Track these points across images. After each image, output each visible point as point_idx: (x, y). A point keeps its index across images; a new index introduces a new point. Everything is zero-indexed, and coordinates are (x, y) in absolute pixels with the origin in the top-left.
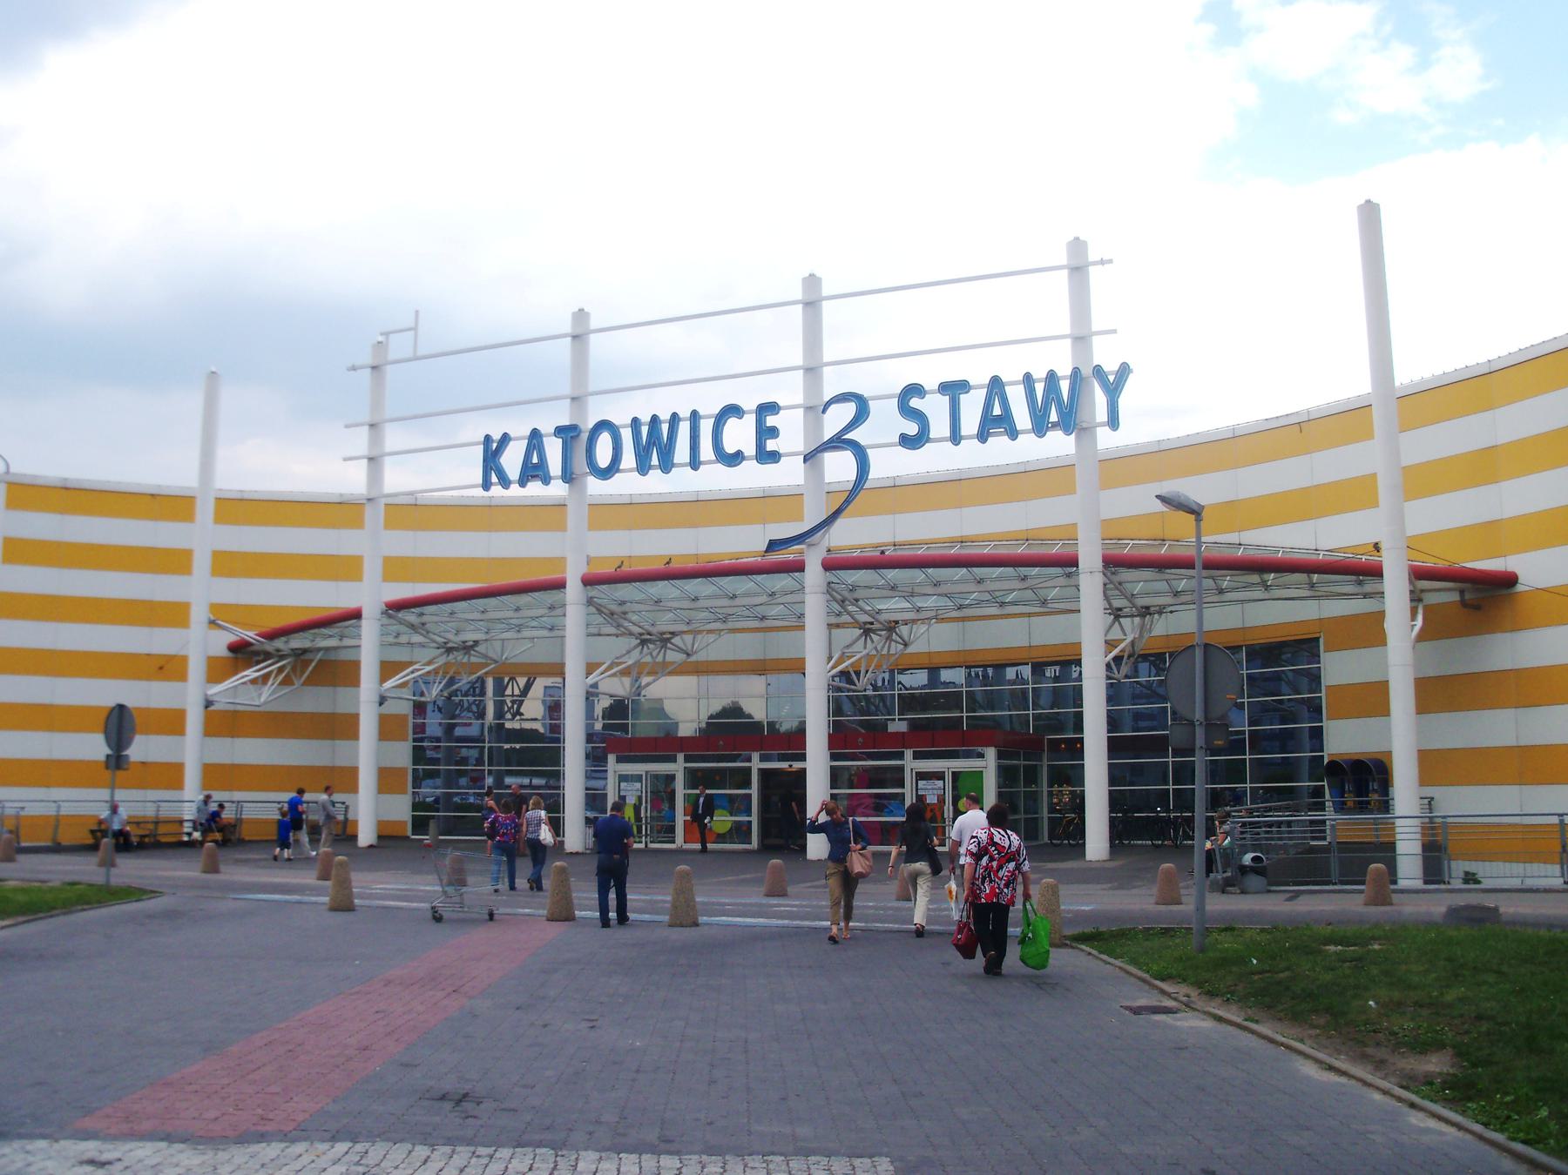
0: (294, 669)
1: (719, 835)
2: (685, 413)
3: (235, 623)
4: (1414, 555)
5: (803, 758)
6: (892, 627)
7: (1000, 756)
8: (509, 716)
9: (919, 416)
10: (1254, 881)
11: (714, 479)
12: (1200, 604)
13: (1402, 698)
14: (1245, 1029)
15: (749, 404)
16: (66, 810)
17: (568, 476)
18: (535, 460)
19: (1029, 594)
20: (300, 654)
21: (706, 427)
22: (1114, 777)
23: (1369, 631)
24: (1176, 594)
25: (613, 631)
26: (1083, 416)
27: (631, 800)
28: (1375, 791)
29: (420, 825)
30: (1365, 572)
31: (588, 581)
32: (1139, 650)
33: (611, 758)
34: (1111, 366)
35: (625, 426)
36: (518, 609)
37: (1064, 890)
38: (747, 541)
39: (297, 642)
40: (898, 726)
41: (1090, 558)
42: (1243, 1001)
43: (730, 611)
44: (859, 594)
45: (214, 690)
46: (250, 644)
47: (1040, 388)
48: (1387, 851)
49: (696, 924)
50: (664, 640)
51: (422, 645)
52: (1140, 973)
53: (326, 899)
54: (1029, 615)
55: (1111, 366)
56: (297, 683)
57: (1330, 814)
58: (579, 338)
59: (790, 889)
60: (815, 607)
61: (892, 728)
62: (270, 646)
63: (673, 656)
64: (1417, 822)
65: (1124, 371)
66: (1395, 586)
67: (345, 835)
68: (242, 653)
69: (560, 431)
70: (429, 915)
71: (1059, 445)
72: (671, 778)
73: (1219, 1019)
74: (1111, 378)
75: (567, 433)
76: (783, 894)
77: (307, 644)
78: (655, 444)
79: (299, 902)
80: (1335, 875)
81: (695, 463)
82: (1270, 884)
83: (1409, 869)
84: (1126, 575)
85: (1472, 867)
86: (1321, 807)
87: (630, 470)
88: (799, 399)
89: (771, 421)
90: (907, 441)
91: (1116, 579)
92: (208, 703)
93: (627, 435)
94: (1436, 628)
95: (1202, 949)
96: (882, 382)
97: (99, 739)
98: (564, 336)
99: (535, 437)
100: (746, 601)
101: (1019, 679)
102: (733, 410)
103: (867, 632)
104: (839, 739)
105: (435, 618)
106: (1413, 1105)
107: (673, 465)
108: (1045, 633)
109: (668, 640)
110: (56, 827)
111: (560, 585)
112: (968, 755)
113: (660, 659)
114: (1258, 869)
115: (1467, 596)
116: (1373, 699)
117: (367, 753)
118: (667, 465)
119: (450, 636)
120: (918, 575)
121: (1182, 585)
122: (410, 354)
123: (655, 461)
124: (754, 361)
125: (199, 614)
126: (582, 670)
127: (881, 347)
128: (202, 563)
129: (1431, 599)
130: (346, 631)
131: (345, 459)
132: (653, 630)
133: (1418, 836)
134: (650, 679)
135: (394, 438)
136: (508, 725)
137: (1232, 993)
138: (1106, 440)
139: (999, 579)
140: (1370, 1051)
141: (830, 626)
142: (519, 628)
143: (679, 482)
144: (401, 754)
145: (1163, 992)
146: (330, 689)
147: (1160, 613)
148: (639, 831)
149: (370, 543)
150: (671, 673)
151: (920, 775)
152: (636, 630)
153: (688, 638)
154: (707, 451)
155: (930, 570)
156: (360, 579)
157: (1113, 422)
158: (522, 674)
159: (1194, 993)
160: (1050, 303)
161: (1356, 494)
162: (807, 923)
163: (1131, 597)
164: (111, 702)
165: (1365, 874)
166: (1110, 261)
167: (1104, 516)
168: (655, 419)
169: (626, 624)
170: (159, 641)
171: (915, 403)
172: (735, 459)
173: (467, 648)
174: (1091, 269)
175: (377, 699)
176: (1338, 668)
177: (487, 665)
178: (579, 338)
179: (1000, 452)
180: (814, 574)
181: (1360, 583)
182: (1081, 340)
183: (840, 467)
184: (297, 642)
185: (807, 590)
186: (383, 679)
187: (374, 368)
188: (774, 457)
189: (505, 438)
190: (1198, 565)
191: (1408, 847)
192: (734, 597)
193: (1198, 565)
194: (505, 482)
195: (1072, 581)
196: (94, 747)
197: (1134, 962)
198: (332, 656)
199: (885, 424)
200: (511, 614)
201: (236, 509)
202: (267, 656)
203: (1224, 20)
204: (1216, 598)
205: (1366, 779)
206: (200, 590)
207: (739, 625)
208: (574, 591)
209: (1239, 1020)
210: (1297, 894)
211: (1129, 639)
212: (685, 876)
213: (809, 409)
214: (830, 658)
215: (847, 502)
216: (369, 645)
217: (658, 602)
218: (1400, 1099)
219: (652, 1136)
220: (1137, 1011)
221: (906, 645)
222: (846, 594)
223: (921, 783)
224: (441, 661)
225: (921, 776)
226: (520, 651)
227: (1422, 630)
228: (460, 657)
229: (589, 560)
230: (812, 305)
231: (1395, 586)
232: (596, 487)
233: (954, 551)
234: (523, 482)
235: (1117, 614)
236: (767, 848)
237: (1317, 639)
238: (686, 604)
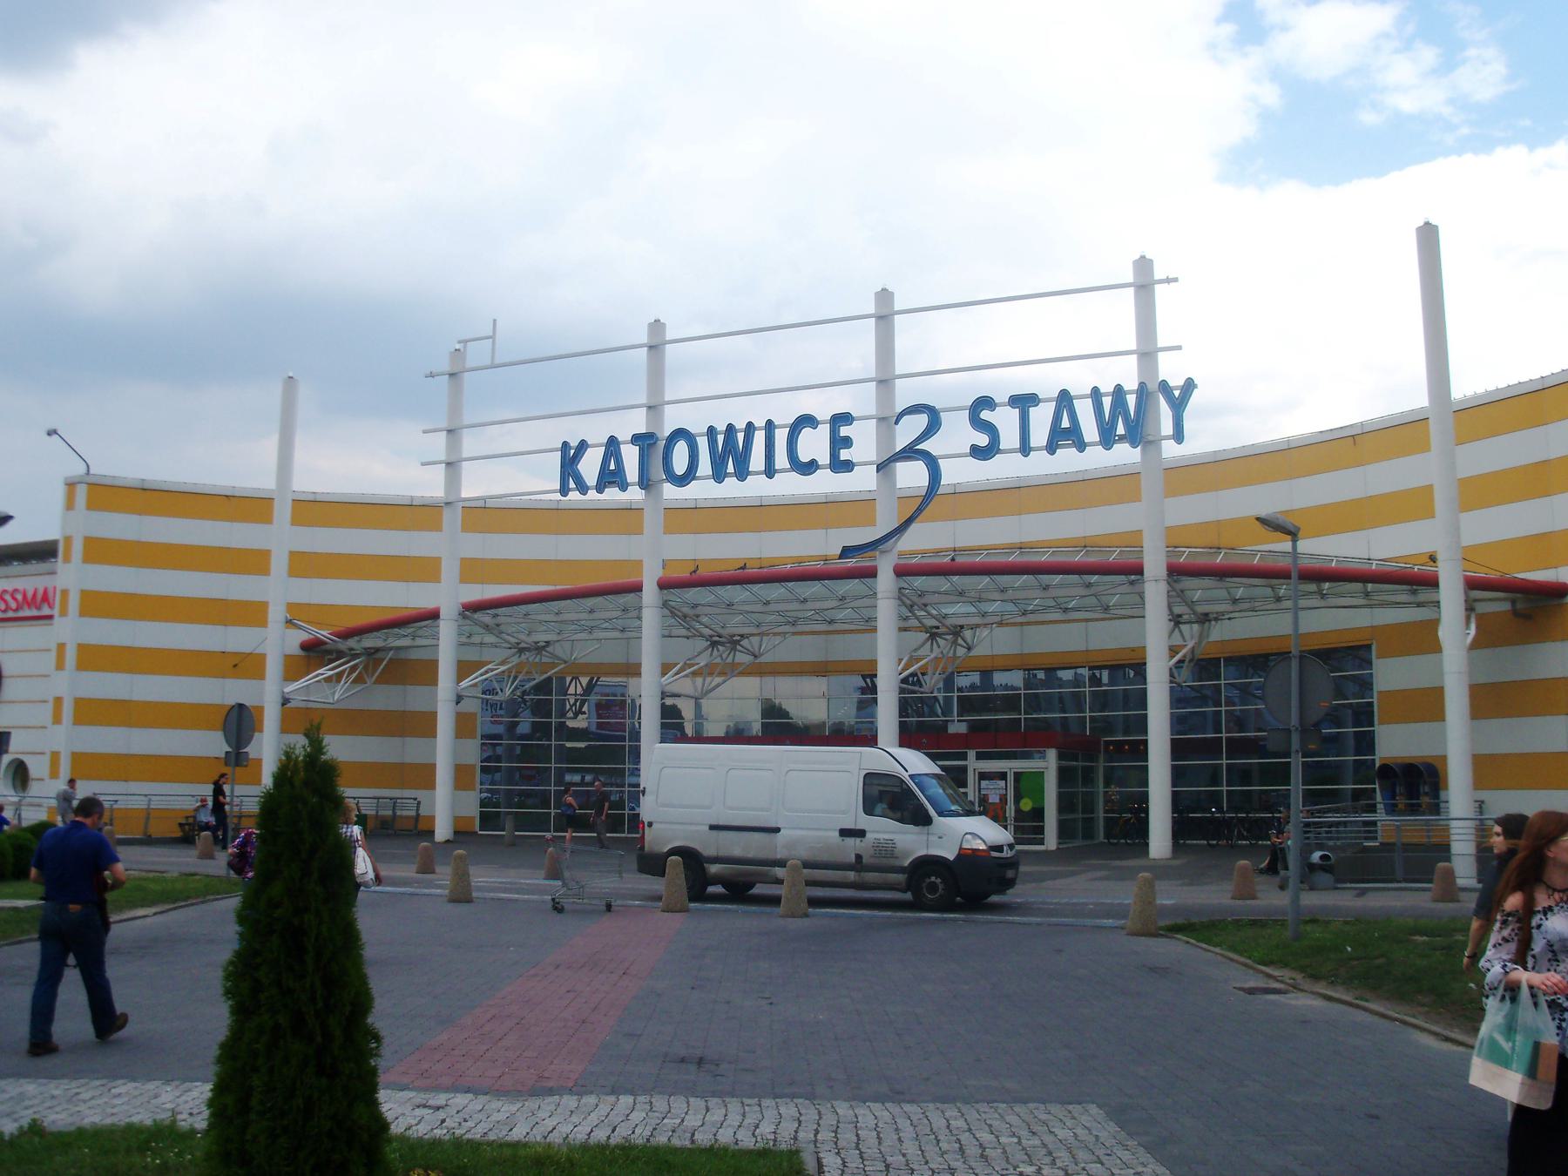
0: (366, 668)
2: (760, 422)
6: (957, 631)
7: (1061, 757)
8: (570, 714)
9: (990, 429)
10: (1324, 878)
11: (789, 485)
14: (1358, 1007)
15: (824, 414)
16: (156, 804)
18: (612, 467)
19: (1093, 600)
20: (371, 653)
21: (781, 436)
22: (1178, 775)
23: (1424, 639)
24: (1235, 601)
25: (684, 632)
28: (1426, 794)
29: (487, 820)
30: (1420, 582)
32: (1198, 655)
34: (1176, 381)
37: (1161, 886)
38: (820, 545)
39: (370, 641)
40: (958, 727)
41: (1155, 565)
42: (1347, 983)
43: (800, 615)
44: (928, 599)
47: (1107, 402)
50: (734, 643)
52: (1242, 959)
54: (1087, 620)
55: (1176, 381)
56: (370, 681)
57: (1381, 816)
58: (655, 348)
60: (886, 612)
61: (952, 729)
62: (343, 645)
63: (742, 658)
65: (1189, 386)
66: (1451, 596)
67: (420, 829)
68: (315, 652)
69: (636, 439)
70: (550, 905)
71: (1125, 455)
74: (1177, 393)
75: (644, 441)
77: (379, 643)
78: (730, 452)
79: (412, 894)
81: (770, 471)
82: (1338, 881)
84: (1188, 583)
86: (1372, 809)
88: (872, 409)
89: (844, 431)
90: (977, 452)
91: (1178, 586)
92: (285, 701)
93: (703, 443)
94: (1488, 637)
96: (952, 393)
99: (612, 445)
100: (818, 605)
101: (1077, 682)
102: (807, 421)
103: (933, 635)
105: (509, 620)
107: (749, 473)
108: (1106, 637)
111: (637, 588)
113: (730, 660)
114: (1326, 866)
115: (1519, 606)
116: (1428, 705)
117: (445, 750)
118: (742, 473)
119: (523, 637)
121: (1240, 593)
122: (488, 362)
123: (730, 469)
124: (822, 373)
125: (276, 614)
128: (279, 563)
129: (1482, 608)
130: (420, 633)
131: (423, 464)
133: (1472, 837)
134: (718, 680)
135: (471, 444)
136: (571, 724)
138: (1170, 450)
139: (1060, 586)
142: (591, 630)
143: (756, 488)
144: (472, 753)
145: (1269, 976)
146: (399, 688)
147: (1216, 619)
150: (742, 674)
152: (707, 632)
153: (755, 640)
154: (781, 460)
155: (955, 578)
157: (1178, 436)
158: (585, 674)
159: (1299, 977)
160: (1115, 321)
161: (1416, 504)
163: (1191, 604)
164: (231, 701)
165: (1432, 872)
166: (1175, 280)
167: (1168, 524)
168: (730, 428)
169: (698, 626)
170: (236, 639)
171: (985, 415)
172: (810, 467)
173: (539, 649)
174: (1157, 287)
175: (280, 701)
176: (1390, 675)
178: (655, 348)
179: (1067, 461)
180: (885, 581)
181: (1414, 592)
182: (1147, 354)
183: (912, 476)
184: (370, 641)
185: (879, 596)
186: (460, 678)
187: (451, 375)
188: (848, 466)
189: (583, 446)
190: (1294, 575)
192: (805, 601)
193: (1294, 575)
194: (583, 488)
197: (1232, 948)
198: (402, 655)
199: (956, 436)
200: (584, 616)
201: (313, 510)
202: (340, 654)
203: (1244, 19)
206: (277, 590)
207: (807, 628)
208: (650, 594)
210: (1362, 893)
211: (1190, 644)
213: (882, 420)
214: (900, 660)
215: (919, 510)
216: (446, 644)
221: (969, 649)
222: (915, 599)
223: (984, 783)
224: (515, 660)
225: (983, 776)
226: (588, 651)
229: (665, 564)
231: (1451, 596)
232: (670, 492)
234: (600, 488)
237: (1369, 647)
238: (759, 608)
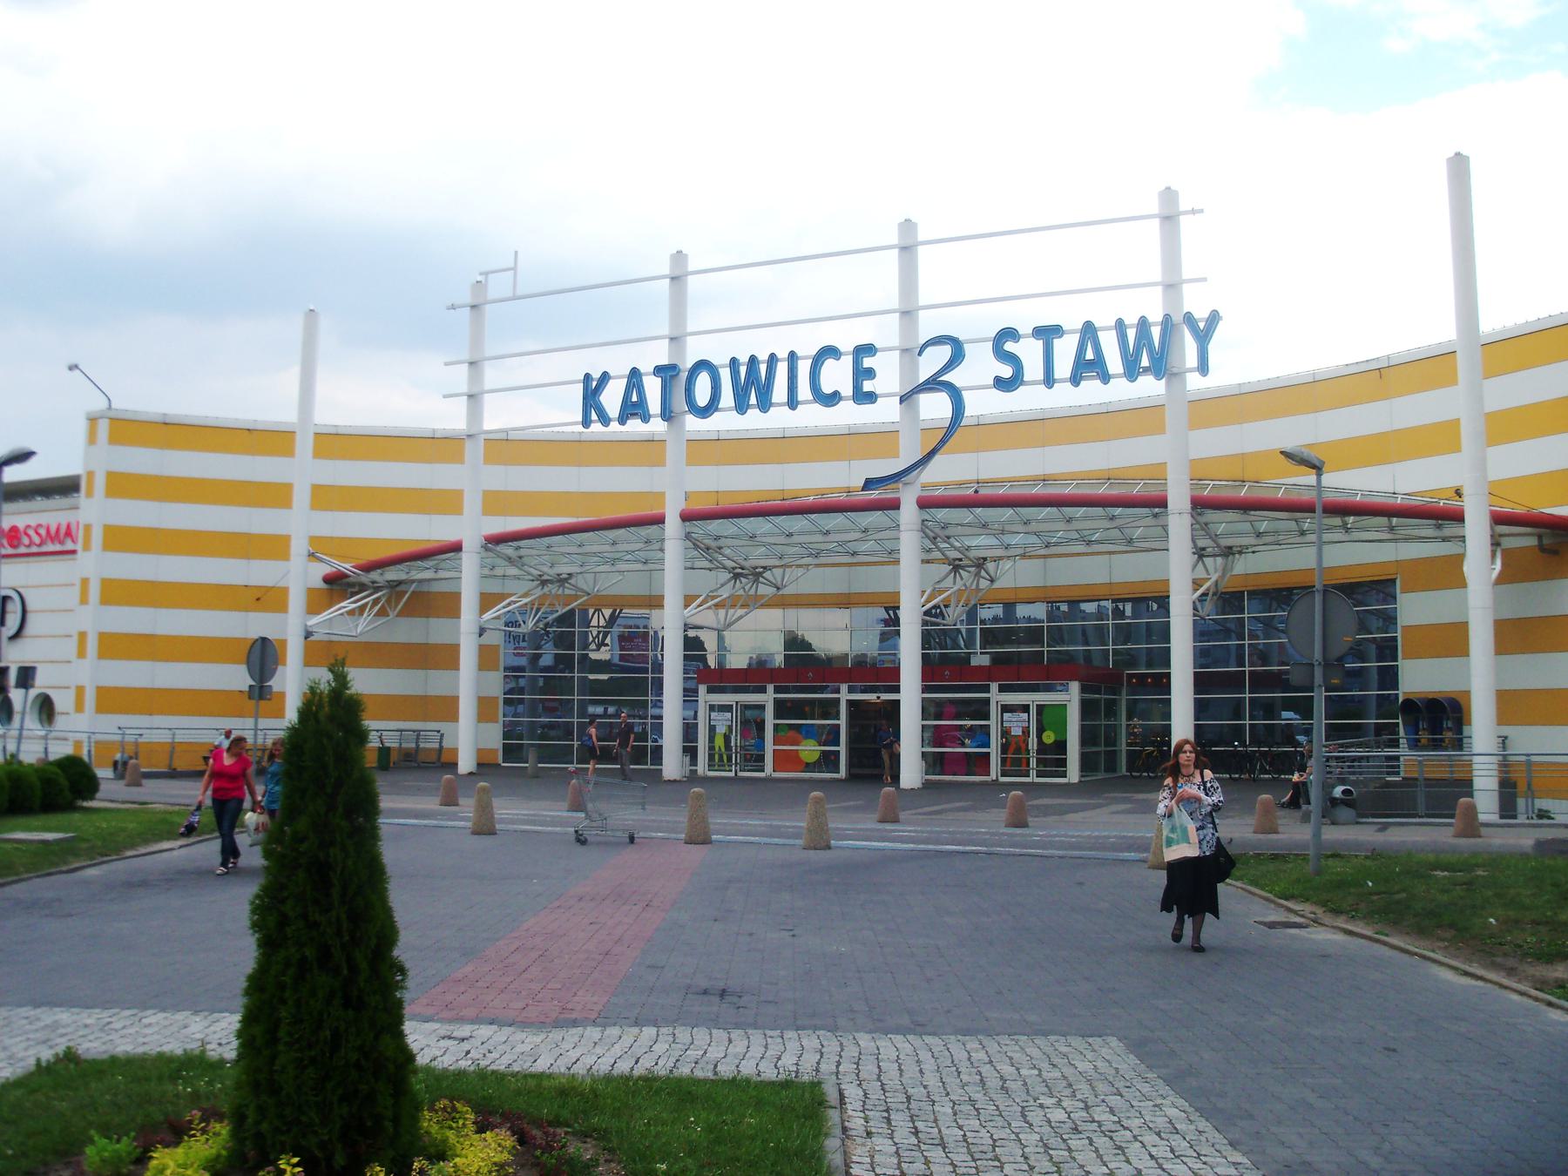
0: (389, 601)
1: (807, 764)
2: (783, 354)
3: (331, 556)
4: (1495, 501)
5: (897, 689)
6: (980, 563)
7: (1083, 690)
8: (593, 646)
9: (1013, 359)
10: (1344, 813)
11: (812, 417)
12: (1320, 544)
13: (1481, 638)
14: (1377, 941)
16: (181, 737)
17: (667, 414)
18: (634, 398)
19: (1116, 533)
20: (394, 586)
21: (804, 368)
23: (1449, 574)
24: (1259, 535)
25: (707, 564)
26: (1173, 361)
27: (721, 730)
28: (1449, 729)
29: (511, 752)
30: (1446, 516)
31: (687, 517)
32: (1221, 589)
33: (702, 689)
34: (1201, 314)
35: (723, 366)
36: (614, 543)
38: (844, 477)
39: (393, 574)
40: (981, 660)
41: (1179, 499)
42: (1368, 917)
43: (822, 546)
45: (314, 621)
46: (347, 576)
47: (1131, 334)
48: (1466, 785)
49: (829, 847)
50: (757, 574)
51: (517, 578)
53: (469, 824)
55: (1201, 314)
57: (1404, 751)
59: (903, 816)
60: (909, 544)
61: (975, 661)
62: (365, 578)
63: (764, 590)
64: (1494, 759)
65: (1214, 318)
66: (1476, 529)
67: (444, 762)
68: (337, 585)
69: (659, 370)
70: (573, 838)
71: (1149, 387)
72: (762, 707)
73: (1350, 933)
74: (1202, 325)
75: (666, 372)
76: (896, 821)
77: (403, 576)
78: (753, 384)
80: (1421, 810)
81: (792, 403)
83: (1485, 800)
84: (1211, 515)
85: (1542, 803)
87: (729, 409)
88: (896, 342)
89: (867, 362)
90: (1001, 384)
91: (1203, 519)
92: (308, 634)
94: (1514, 571)
95: (1318, 873)
96: (977, 325)
97: (242, 670)
98: (663, 277)
99: (635, 376)
101: (1100, 615)
102: (829, 352)
104: (932, 670)
106: (1550, 1004)
107: (771, 405)
108: (1129, 570)
109: (760, 574)
110: (172, 753)
111: (659, 520)
112: (1049, 689)
113: (752, 592)
114: (1348, 801)
115: (1545, 541)
116: (1452, 640)
117: (468, 683)
118: (765, 404)
119: (545, 569)
120: (1009, 512)
121: (1263, 526)
122: (510, 294)
123: (753, 400)
124: (841, 303)
125: (299, 547)
126: (681, 602)
127: (968, 291)
128: (301, 496)
129: (1508, 543)
130: (443, 565)
132: (746, 564)
133: (1495, 773)
134: (740, 612)
135: (492, 375)
136: (594, 656)
137: (1356, 910)
138: (1195, 383)
139: (1085, 518)
140: (1499, 960)
141: (923, 561)
142: (614, 562)
143: (778, 419)
144: (495, 684)
145: (1289, 910)
147: (1240, 553)
148: (730, 759)
149: (471, 477)
150: (763, 606)
151: (1009, 711)
152: (730, 564)
154: (804, 391)
155: (979, 510)
156: (461, 513)
157: (1203, 368)
159: (1319, 911)
160: (1141, 251)
161: (1442, 438)
162: (931, 847)
163: (1214, 538)
164: (254, 633)
166: (1201, 211)
167: (1193, 456)
168: (753, 359)
169: (720, 558)
170: (259, 573)
171: (1009, 346)
172: (832, 399)
173: (562, 581)
175: (303, 634)
176: (1414, 609)
177: (576, 597)
180: (909, 513)
181: (1439, 527)
182: (1172, 287)
183: (935, 407)
184: (393, 574)
187: (473, 307)
188: (871, 397)
189: (605, 377)
190: (1319, 509)
191: (1485, 782)
193: (1319, 509)
195: (1160, 521)
196: (237, 678)
197: (1254, 883)
198: (425, 588)
199: (979, 368)
201: (334, 444)
202: (362, 587)
204: (1298, 539)
205: (1441, 718)
206: (299, 523)
207: (830, 560)
208: (673, 525)
209: (1369, 933)
210: (1384, 827)
211: (1214, 577)
212: (818, 801)
213: (905, 351)
215: (943, 441)
216: (469, 577)
217: (753, 537)
218: (1536, 999)
219: (905, 1020)
220: (1272, 925)
221: (992, 581)
224: (538, 592)
225: (1006, 709)
226: (612, 582)
227: (1501, 573)
228: (552, 589)
229: (687, 496)
230: (907, 250)
231: (1476, 529)
233: (1037, 490)
234: (622, 420)
235: (1200, 554)
236: (853, 777)
237: (1393, 581)
238: (782, 540)
